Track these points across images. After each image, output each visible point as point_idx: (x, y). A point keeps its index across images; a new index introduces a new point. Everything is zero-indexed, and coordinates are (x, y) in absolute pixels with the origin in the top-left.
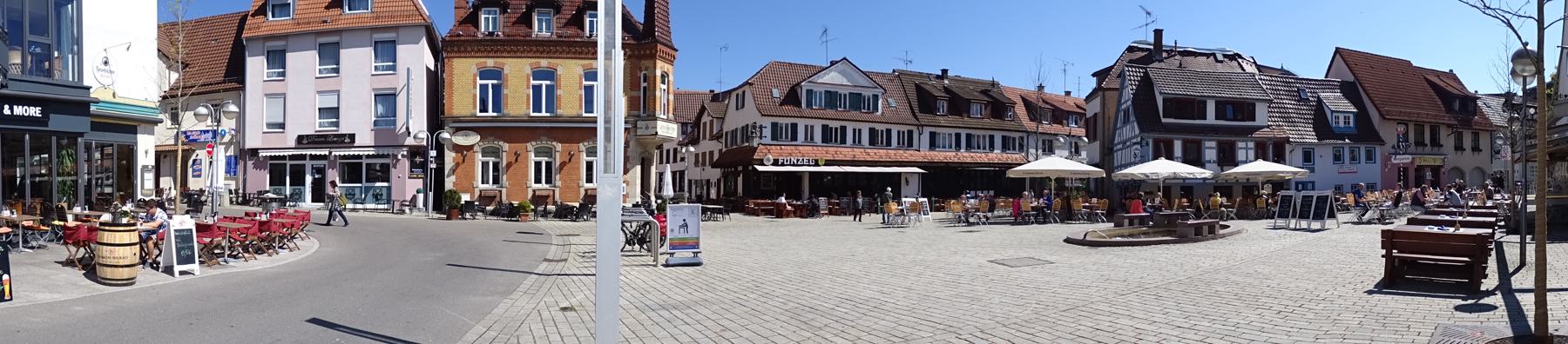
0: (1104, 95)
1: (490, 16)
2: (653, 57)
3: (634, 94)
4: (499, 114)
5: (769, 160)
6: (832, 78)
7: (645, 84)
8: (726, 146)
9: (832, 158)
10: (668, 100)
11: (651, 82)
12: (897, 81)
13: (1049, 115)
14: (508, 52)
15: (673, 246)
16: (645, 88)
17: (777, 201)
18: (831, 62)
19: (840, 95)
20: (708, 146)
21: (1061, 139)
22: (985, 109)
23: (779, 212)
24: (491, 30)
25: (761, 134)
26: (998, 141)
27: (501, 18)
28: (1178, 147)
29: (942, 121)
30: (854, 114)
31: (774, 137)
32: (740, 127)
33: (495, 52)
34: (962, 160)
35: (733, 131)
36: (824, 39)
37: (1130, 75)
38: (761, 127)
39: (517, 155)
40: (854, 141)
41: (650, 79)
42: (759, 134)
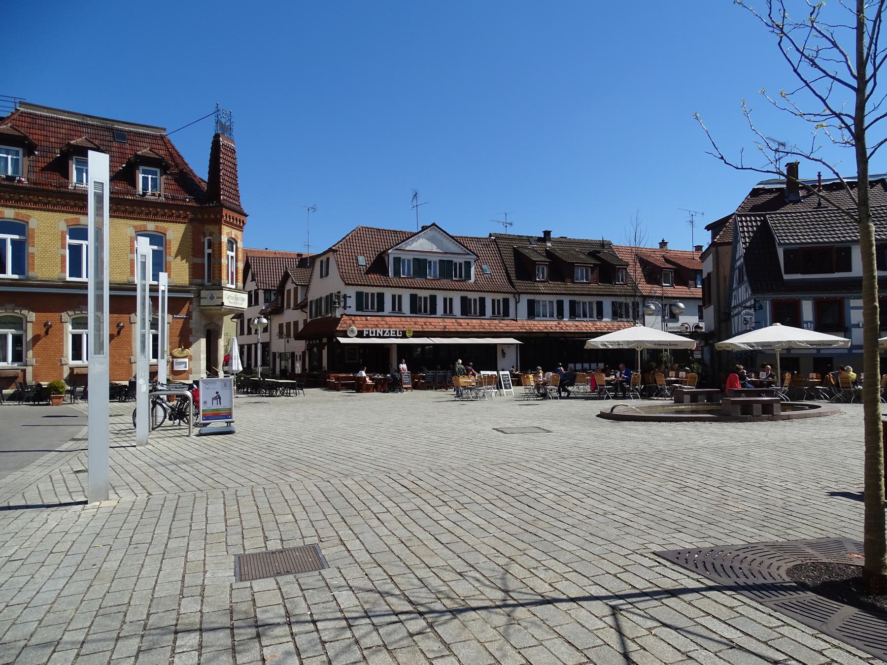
1: (10, 157)
2: (218, 222)
3: (198, 260)
4: (22, 277)
5: (352, 331)
6: (421, 245)
7: (210, 251)
8: (311, 317)
9: (421, 330)
10: (237, 268)
12: (493, 246)
14: (35, 203)
16: (209, 255)
17: (358, 375)
20: (291, 316)
22: (592, 273)
23: (359, 387)
24: (10, 173)
25: (345, 304)
27: (24, 162)
28: (807, 310)
29: (542, 287)
30: (446, 282)
31: (359, 307)
32: (324, 295)
33: (17, 201)
34: (565, 330)
35: (317, 300)
36: (415, 203)
39: (47, 327)
41: (216, 247)
42: (342, 304)
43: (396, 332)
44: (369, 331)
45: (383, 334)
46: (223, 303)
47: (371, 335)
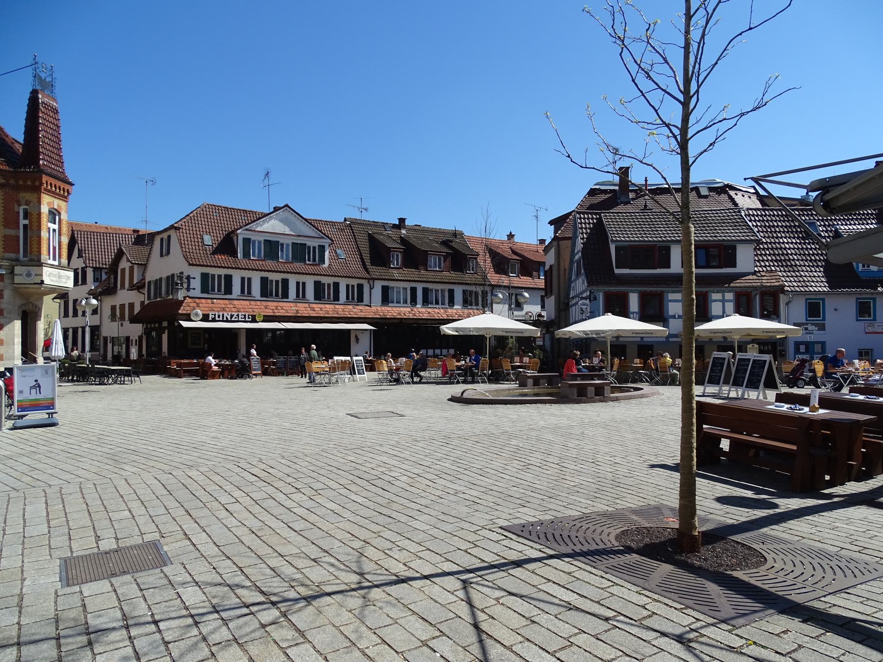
0: (559, 246)
5: (197, 314)
6: (273, 226)
7: (26, 222)
8: (149, 298)
9: (272, 314)
10: (60, 243)
11: (34, 220)
12: (348, 230)
13: (517, 266)
15: (22, 408)
16: (25, 226)
18: (274, 208)
19: (309, 247)
20: (125, 297)
21: (526, 295)
22: (444, 262)
23: (204, 373)
26: (458, 296)
28: (634, 302)
29: (396, 274)
30: (298, 266)
31: (205, 289)
32: (164, 276)
34: (418, 316)
35: (156, 280)
36: (266, 182)
37: (581, 223)
38: (188, 278)
40: (298, 296)
42: (185, 286)
43: (245, 316)
44: (215, 315)
45: (231, 318)
46: (42, 282)
47: (217, 319)
